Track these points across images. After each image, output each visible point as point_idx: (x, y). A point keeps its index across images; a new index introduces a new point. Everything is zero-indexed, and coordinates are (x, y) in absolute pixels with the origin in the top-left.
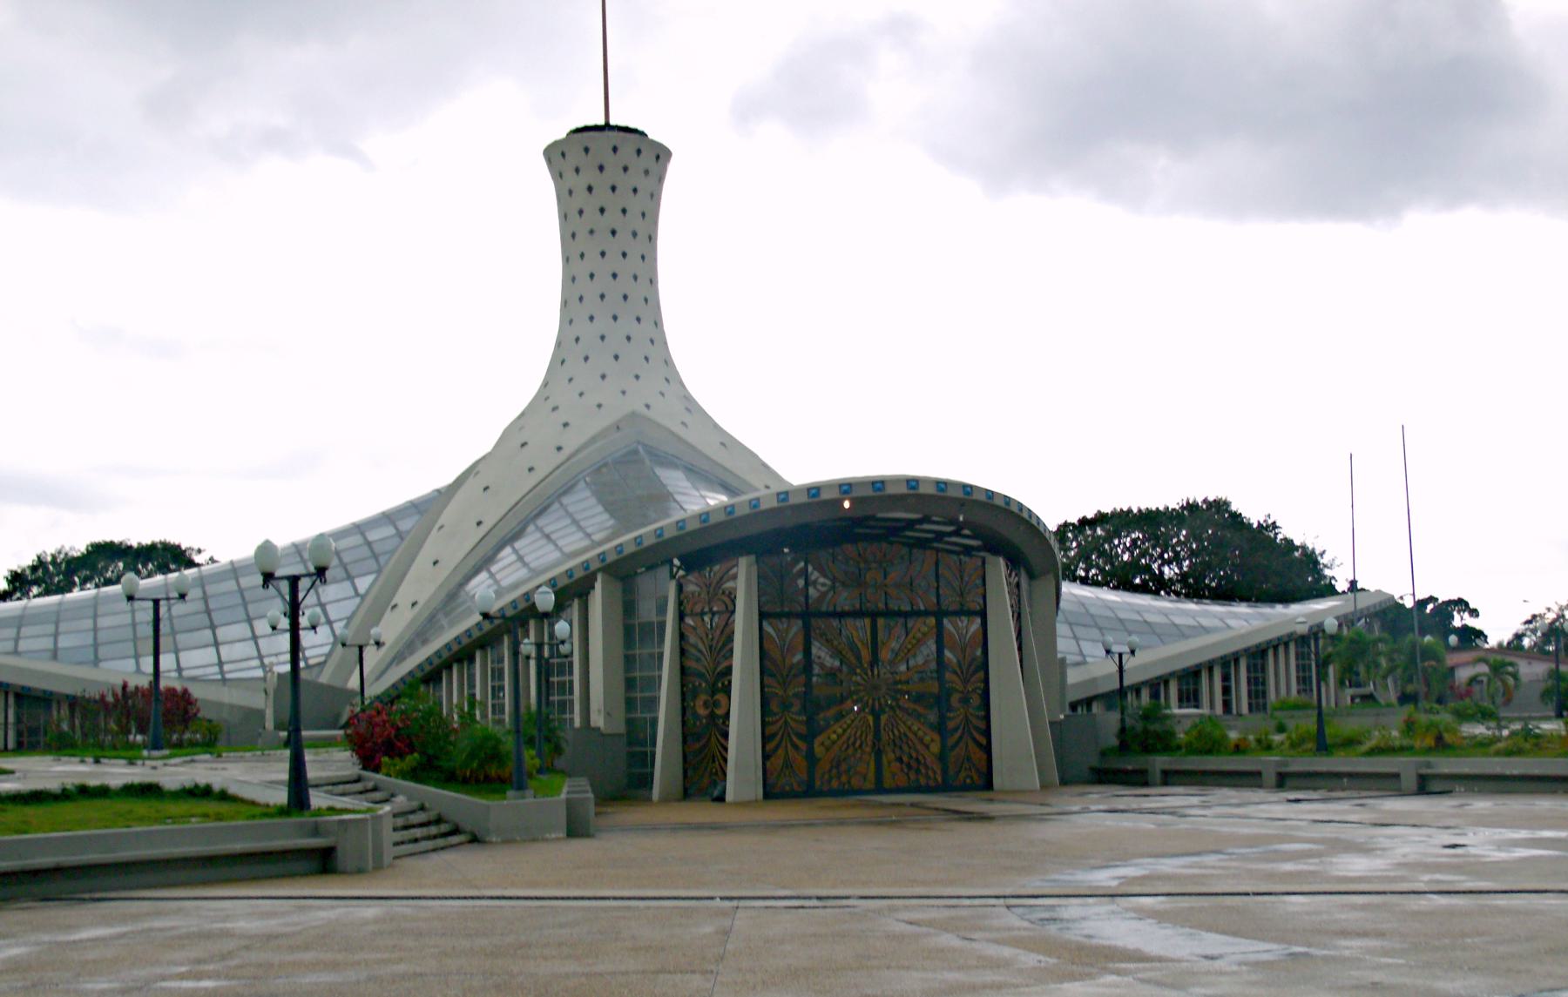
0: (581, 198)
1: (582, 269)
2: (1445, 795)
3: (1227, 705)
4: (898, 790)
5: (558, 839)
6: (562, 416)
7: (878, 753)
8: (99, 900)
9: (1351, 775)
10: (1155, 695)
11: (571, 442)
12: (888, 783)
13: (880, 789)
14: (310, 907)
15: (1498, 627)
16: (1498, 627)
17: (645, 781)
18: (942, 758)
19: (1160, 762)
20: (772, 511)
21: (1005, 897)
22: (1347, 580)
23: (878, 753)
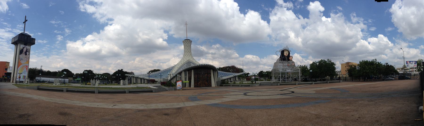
0: (185, 44)
1: (185, 49)
2: (41, 90)
3: (233, 80)
4: (204, 87)
5: (174, 91)
6: (186, 58)
7: (203, 84)
8: (117, 95)
9: (237, 86)
10: (228, 80)
11: (184, 61)
12: (204, 86)
13: (203, 87)
14: (198, 94)
15: (111, 74)
16: (111, 74)
17: (186, 86)
18: (208, 84)
19: (224, 85)
20: (201, 66)
21: (330, 94)
22: (93, 71)
23: (203, 84)
